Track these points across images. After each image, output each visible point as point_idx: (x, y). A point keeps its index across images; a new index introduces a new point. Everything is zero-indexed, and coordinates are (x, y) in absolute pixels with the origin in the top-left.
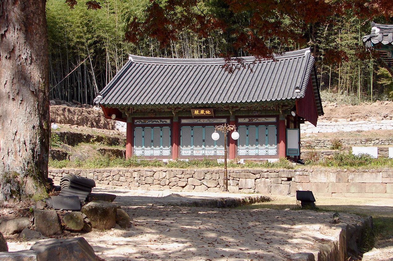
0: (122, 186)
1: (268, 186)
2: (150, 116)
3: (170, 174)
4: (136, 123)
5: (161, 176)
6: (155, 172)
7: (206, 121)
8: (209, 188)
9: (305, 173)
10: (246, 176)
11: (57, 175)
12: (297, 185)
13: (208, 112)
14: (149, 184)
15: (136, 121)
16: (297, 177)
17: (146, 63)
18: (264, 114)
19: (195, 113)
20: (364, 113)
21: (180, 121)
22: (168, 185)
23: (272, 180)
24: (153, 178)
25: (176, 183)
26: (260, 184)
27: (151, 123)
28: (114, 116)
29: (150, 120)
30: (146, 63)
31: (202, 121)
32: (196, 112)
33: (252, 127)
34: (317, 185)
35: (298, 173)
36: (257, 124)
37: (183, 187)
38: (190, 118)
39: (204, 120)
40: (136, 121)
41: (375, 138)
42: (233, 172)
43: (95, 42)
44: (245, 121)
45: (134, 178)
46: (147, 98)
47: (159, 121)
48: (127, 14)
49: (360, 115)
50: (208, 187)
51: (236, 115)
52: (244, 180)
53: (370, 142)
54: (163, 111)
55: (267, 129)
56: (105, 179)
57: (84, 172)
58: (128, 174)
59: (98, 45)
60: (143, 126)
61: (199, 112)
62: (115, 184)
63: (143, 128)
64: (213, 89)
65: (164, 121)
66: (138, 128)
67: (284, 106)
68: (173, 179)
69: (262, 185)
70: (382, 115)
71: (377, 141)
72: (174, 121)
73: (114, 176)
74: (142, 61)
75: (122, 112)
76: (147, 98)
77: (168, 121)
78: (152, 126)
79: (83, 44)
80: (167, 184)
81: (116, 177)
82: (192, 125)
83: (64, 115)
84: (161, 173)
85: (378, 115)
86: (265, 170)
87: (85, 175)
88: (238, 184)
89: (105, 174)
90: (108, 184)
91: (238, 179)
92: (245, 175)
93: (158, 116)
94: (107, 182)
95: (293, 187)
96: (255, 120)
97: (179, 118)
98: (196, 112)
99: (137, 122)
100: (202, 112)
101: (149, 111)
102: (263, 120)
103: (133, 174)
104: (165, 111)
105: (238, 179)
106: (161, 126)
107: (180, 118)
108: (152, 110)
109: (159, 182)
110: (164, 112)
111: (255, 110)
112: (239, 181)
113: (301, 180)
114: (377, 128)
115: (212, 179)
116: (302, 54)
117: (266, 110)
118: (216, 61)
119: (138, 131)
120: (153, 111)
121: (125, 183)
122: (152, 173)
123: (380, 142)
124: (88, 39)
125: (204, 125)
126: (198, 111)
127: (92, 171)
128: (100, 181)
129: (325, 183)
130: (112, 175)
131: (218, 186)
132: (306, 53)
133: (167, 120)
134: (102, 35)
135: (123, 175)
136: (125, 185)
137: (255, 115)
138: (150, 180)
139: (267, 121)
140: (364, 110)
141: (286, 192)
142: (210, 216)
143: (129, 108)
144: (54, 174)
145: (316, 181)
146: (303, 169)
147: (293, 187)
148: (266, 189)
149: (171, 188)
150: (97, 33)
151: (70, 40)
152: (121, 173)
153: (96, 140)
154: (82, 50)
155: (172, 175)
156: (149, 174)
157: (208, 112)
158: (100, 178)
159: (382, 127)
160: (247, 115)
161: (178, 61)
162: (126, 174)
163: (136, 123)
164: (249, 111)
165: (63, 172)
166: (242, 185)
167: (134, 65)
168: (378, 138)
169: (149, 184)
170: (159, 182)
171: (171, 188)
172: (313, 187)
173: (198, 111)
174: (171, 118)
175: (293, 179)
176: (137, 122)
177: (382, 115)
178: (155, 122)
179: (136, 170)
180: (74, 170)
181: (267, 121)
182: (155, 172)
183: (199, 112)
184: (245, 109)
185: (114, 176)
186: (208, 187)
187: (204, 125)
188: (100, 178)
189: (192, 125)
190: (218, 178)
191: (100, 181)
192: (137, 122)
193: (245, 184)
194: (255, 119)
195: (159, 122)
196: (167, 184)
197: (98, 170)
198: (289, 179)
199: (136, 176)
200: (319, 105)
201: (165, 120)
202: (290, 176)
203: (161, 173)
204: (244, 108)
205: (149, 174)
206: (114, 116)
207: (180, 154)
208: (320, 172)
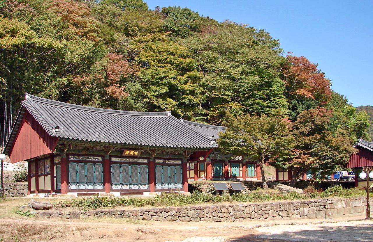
0: (221, 221)
2: (84, 153)
4: (70, 158)
5: (251, 210)
7: (131, 160)
8: (283, 218)
10: (304, 206)
27: (84, 159)
29: (84, 157)
31: (129, 160)
32: (127, 153)
34: (338, 210)
36: (169, 165)
37: (266, 218)
39: (130, 159)
40: (70, 157)
44: (160, 162)
47: (92, 158)
50: (282, 217)
54: (95, 149)
60: (78, 162)
63: (175, 167)
65: (97, 158)
66: (72, 163)
69: (312, 213)
73: (212, 212)
74: (40, 101)
78: (86, 162)
93: (91, 153)
96: (168, 162)
97: (109, 157)
98: (127, 153)
99: (71, 158)
100: (132, 153)
101: (82, 148)
102: (172, 162)
104: (97, 149)
106: (94, 162)
107: (111, 157)
110: (96, 150)
111: (167, 154)
113: (330, 207)
116: (166, 115)
117: (174, 154)
118: (113, 112)
120: (86, 149)
125: (130, 164)
127: (193, 209)
129: (341, 208)
130: (211, 211)
133: (99, 158)
139: (175, 163)
160: (162, 157)
163: (70, 158)
164: (163, 154)
169: (242, 218)
170: (249, 216)
174: (103, 157)
176: (71, 157)
178: (88, 159)
179: (231, 206)
181: (175, 163)
187: (130, 164)
189: (121, 163)
192: (71, 157)
194: (168, 161)
195: (92, 159)
200: (7, 147)
201: (98, 158)
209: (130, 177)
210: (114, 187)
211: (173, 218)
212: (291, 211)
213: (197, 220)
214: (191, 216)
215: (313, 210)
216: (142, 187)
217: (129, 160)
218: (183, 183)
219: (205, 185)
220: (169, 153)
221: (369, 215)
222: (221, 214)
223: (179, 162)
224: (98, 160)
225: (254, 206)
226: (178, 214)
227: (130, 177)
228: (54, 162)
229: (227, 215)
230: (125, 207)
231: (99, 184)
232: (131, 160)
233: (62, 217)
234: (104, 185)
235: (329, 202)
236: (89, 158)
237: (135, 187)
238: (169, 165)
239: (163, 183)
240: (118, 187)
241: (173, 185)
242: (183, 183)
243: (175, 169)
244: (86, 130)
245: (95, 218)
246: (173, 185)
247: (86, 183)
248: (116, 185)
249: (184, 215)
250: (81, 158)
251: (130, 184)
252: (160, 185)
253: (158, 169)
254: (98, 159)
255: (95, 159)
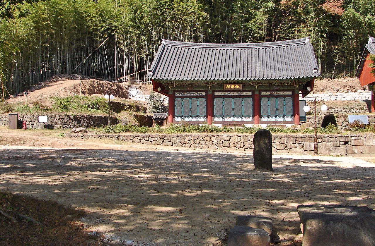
0: (202, 148)
1: (329, 149)
3: (244, 139)
6: (231, 137)
7: (235, 94)
9: (360, 138)
11: (144, 139)
12: (353, 148)
13: (237, 87)
14: (226, 147)
15: (176, 93)
16: (353, 141)
17: (176, 46)
18: (283, 89)
19: (227, 87)
20: (321, 88)
21: (260, 93)
22: (243, 148)
23: (332, 143)
24: (229, 142)
25: (250, 146)
26: (321, 147)
28: (159, 89)
30: (176, 46)
31: (232, 94)
32: (228, 87)
33: (272, 99)
34: (370, 148)
35: (353, 138)
36: (277, 97)
38: (223, 91)
39: (234, 93)
40: (176, 93)
41: (335, 107)
42: (299, 137)
43: (108, 29)
44: (267, 94)
45: (213, 142)
46: (195, 73)
48: (135, 8)
49: (318, 89)
50: (277, 150)
51: (260, 89)
52: (308, 144)
53: (331, 110)
54: (199, 85)
55: (285, 100)
56: (187, 142)
57: (168, 137)
58: (208, 139)
59: (110, 31)
60: (183, 97)
61: (230, 87)
62: (196, 147)
64: (196, 68)
65: (200, 93)
67: (299, 82)
68: (247, 143)
70: (335, 90)
71: (337, 109)
72: (209, 93)
73: (194, 140)
75: (165, 85)
76: (195, 73)
77: (204, 94)
78: (190, 97)
79: (98, 30)
80: (242, 147)
81: (197, 141)
82: (223, 97)
83: (98, 87)
84: (236, 138)
85: (332, 89)
86: (326, 135)
87: (169, 139)
88: (303, 147)
89: (187, 139)
90: (190, 147)
91: (303, 143)
92: (309, 140)
93: (195, 89)
94: (189, 145)
95: (349, 150)
96: (275, 94)
98: (228, 87)
100: (233, 86)
101: (187, 85)
102: (281, 93)
103: (212, 138)
105: (303, 143)
106: (198, 97)
107: (214, 91)
108: (190, 84)
109: (234, 145)
110: (200, 86)
111: (275, 86)
112: (304, 144)
113: (356, 144)
114: (333, 99)
115: (281, 143)
117: (283, 86)
119: (178, 102)
121: (205, 146)
122: (229, 138)
123: (339, 110)
124: (102, 27)
125: (233, 97)
126: (229, 85)
128: (183, 144)
130: (193, 139)
131: (286, 148)
132: (306, 42)
133: (202, 93)
134: (113, 23)
135: (203, 139)
136: (205, 148)
137: (275, 89)
138: (227, 144)
140: (321, 85)
141: (343, 153)
142: (219, 168)
143: (172, 82)
144: (141, 138)
145: (369, 144)
146: (358, 135)
147: (349, 150)
148: (327, 151)
149: (245, 150)
150: (109, 22)
151: (88, 27)
152: (201, 138)
153: (128, 108)
154: (97, 35)
155: (246, 139)
156: (226, 138)
157: (237, 87)
158: (182, 141)
159: (337, 99)
161: (203, 45)
162: (205, 139)
164: (270, 86)
165: (149, 137)
166: (306, 148)
167: (166, 47)
168: (337, 106)
169: (226, 147)
170: (234, 145)
171: (245, 150)
172: (366, 149)
173: (229, 85)
174: (206, 91)
175: (349, 143)
176: (177, 94)
177: (335, 90)
180: (159, 135)
182: (231, 137)
183: (230, 87)
184: (267, 85)
185: (194, 140)
186: (277, 150)
187: (233, 97)
188: (182, 142)
189: (223, 97)
190: (286, 142)
191: (183, 144)
192: (177, 94)
193: (309, 146)
195: (196, 94)
196: (242, 146)
197: (181, 135)
198: (346, 143)
199: (214, 140)
202: (347, 141)
203: (236, 138)
204: (266, 83)
205: (226, 138)
206: (159, 89)
207: (214, 120)
208: (372, 137)
209: (233, 109)
210: (217, 119)
211: (157, 143)
212: (289, 144)
213: (178, 146)
214: (173, 142)
215: (326, 145)
216: (246, 120)
217: (232, 94)
218: (294, 115)
219: (343, 118)
220: (277, 85)
221: (257, 149)
222: (202, 142)
223: (290, 93)
224: (202, 95)
225: (240, 137)
226: (162, 140)
227: (233, 109)
228: (261, 94)
229: (208, 143)
230: (29, 131)
231: (202, 117)
232: (235, 94)
233: (78, 138)
234: (207, 117)
235: (353, 138)
236: (193, 94)
237: (238, 119)
238: (277, 97)
239: (285, 116)
240: (221, 119)
241: (282, 118)
242: (294, 115)
243: (285, 100)
244: (188, 69)
245: (98, 140)
246: (282, 118)
247: (190, 116)
248: (219, 117)
249: (168, 141)
250: (187, 94)
251: (233, 116)
252: (266, 118)
253: (264, 101)
254: (201, 94)
255: (199, 94)
